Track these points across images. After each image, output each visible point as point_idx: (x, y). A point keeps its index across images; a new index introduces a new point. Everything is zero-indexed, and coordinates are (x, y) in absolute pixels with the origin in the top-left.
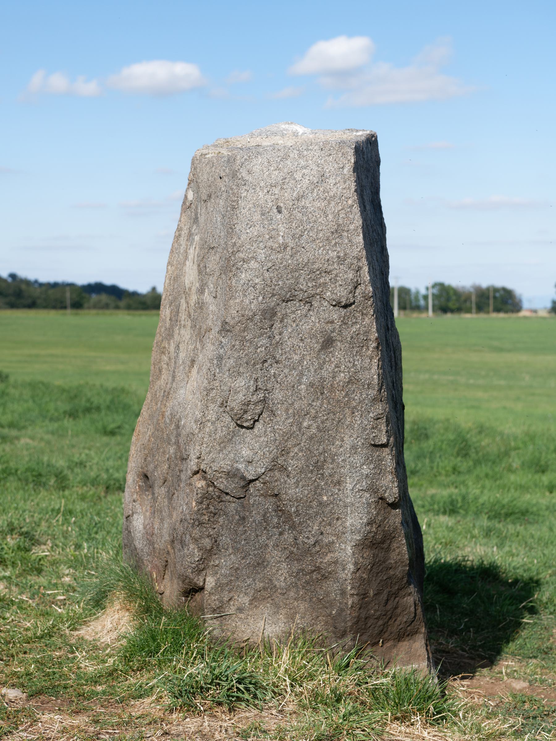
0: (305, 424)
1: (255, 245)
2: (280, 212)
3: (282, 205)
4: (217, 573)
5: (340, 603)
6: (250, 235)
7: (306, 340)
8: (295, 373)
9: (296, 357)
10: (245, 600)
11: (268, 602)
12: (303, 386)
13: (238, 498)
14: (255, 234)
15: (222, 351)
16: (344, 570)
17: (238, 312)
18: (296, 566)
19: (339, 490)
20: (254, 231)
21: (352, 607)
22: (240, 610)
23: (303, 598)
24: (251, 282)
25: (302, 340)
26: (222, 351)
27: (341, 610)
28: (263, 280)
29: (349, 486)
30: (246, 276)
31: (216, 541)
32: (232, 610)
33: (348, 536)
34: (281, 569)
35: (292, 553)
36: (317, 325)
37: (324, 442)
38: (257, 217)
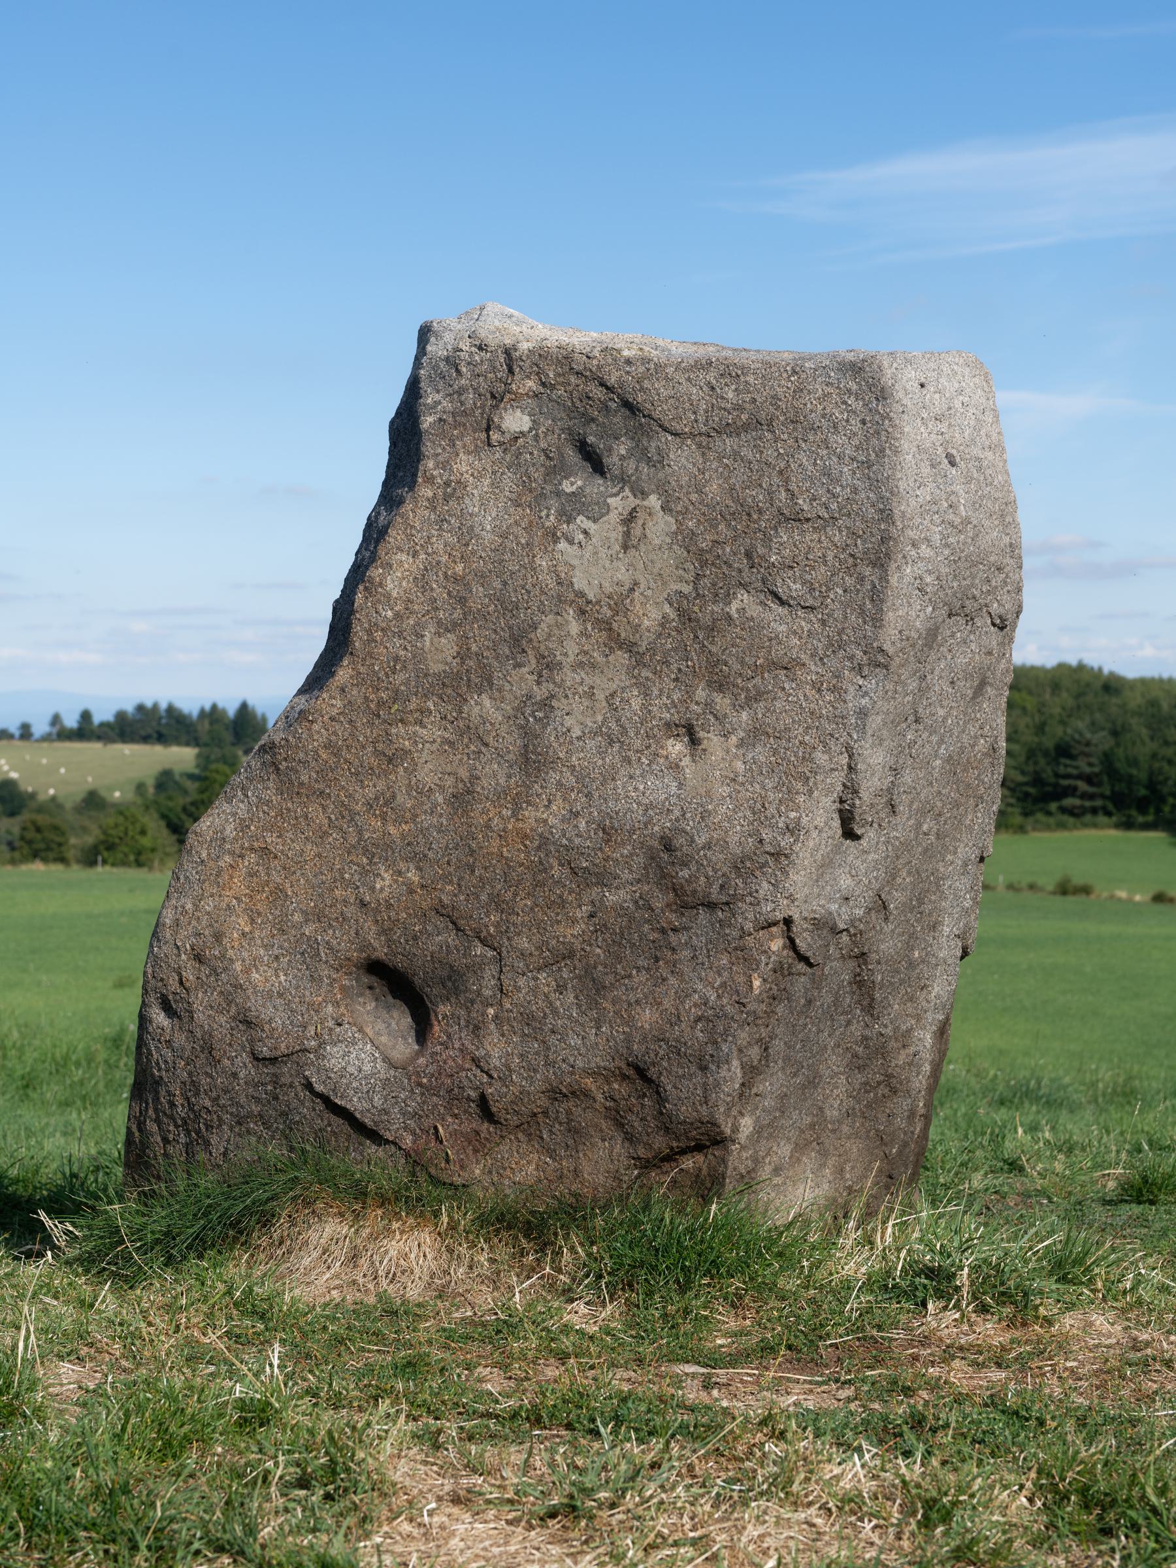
0: (925, 827)
1: (928, 518)
2: (953, 464)
3: (954, 452)
4: (757, 1108)
5: (905, 1133)
6: (920, 500)
7: (958, 683)
8: (935, 738)
9: (941, 712)
10: (784, 1150)
11: (813, 1149)
12: (938, 762)
13: (181, 983)
14: (928, 498)
15: (864, 701)
16: (918, 1074)
17: (900, 632)
18: (859, 1078)
19: (934, 938)
20: (924, 494)
21: (42, 1083)
22: (777, 1171)
23: (856, 1135)
24: (918, 581)
25: (952, 683)
26: (864, 701)
27: (905, 1144)
28: (938, 578)
29: (947, 930)
30: (913, 571)
31: (766, 1049)
32: (765, 1172)
33: (929, 1016)
34: (837, 1088)
35: (855, 1056)
36: (977, 657)
37: (935, 856)
38: (926, 470)
